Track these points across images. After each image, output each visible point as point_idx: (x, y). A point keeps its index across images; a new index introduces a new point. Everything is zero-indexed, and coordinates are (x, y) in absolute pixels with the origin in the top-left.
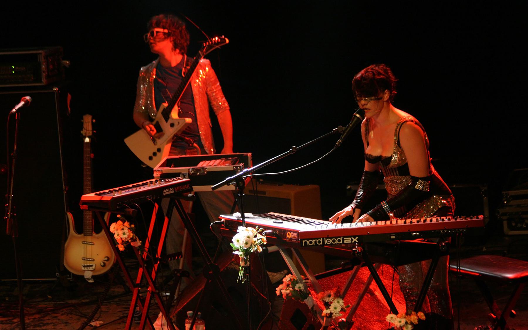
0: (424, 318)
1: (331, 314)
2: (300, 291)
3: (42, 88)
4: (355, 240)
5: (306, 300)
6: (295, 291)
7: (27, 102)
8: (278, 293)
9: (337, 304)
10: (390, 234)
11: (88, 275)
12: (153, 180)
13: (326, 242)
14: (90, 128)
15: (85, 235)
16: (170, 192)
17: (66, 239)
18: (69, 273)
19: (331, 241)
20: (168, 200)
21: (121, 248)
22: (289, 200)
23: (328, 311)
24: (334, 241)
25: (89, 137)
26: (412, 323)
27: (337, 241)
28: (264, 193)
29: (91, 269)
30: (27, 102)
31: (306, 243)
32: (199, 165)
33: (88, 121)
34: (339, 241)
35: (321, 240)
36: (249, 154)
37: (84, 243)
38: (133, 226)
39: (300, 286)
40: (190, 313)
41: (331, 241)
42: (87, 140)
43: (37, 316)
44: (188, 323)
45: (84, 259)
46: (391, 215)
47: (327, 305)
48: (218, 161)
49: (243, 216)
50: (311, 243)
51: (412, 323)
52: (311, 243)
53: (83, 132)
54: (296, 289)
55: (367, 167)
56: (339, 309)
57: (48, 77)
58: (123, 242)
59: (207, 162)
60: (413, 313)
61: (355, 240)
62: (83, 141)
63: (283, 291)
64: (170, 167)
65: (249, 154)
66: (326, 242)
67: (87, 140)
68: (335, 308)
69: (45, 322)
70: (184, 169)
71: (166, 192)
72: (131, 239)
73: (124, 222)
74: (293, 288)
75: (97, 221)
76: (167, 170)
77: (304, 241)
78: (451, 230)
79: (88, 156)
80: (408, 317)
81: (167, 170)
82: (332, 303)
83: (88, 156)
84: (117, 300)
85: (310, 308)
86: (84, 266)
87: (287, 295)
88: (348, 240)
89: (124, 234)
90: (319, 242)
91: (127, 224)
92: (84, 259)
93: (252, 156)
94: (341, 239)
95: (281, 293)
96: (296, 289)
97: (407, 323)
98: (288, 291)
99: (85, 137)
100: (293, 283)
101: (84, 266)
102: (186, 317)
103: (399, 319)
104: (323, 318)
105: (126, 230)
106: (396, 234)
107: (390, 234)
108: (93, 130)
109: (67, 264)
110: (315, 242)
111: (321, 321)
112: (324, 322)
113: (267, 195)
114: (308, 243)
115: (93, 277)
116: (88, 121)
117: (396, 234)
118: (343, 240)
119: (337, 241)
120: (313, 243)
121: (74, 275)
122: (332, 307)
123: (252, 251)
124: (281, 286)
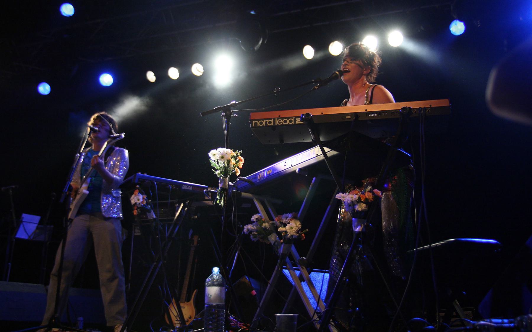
7: (143, 173)
19: (282, 121)
20: (43, 324)
23: (284, 229)
24: (285, 122)
30: (143, 173)
34: (291, 121)
35: (272, 121)
41: (282, 121)
46: (309, 52)
50: (261, 123)
55: (135, 212)
66: (277, 122)
77: (254, 122)
90: (270, 123)
94: (293, 120)
110: (266, 122)
114: (258, 123)
120: (264, 123)
122: (288, 227)
123: (52, 226)
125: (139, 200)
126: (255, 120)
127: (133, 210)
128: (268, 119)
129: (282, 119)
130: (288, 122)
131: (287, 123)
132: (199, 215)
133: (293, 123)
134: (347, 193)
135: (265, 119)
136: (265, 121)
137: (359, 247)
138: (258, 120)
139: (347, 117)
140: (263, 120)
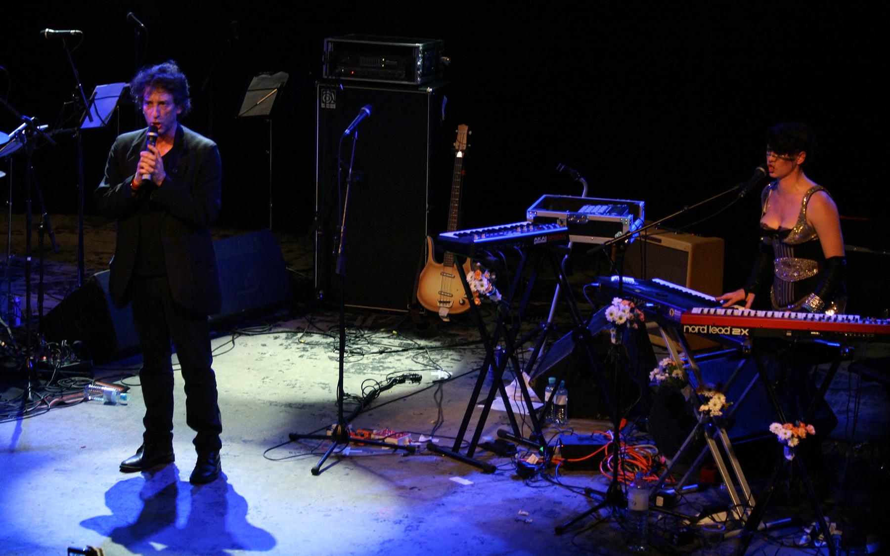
0: (814, 432)
1: (709, 411)
2: (678, 378)
3: (416, 87)
4: (745, 332)
5: (682, 391)
6: (671, 377)
8: (651, 377)
9: (717, 401)
10: (786, 330)
11: (444, 312)
12: (525, 223)
13: (711, 330)
14: (465, 141)
15: (445, 266)
16: (542, 241)
17: (423, 266)
18: (423, 308)
21: (477, 302)
22: (687, 253)
24: (720, 331)
25: (462, 151)
26: (798, 437)
27: (723, 331)
28: (660, 241)
29: (448, 306)
31: (687, 329)
32: (581, 211)
33: (463, 132)
34: (726, 331)
36: (642, 204)
37: (442, 274)
38: (494, 277)
39: (678, 373)
40: (551, 380)
41: (717, 330)
42: (460, 155)
43: (379, 356)
44: (549, 391)
45: (440, 293)
47: (706, 400)
48: (605, 207)
49: (621, 279)
50: (693, 329)
51: (798, 437)
52: (693, 329)
53: (456, 145)
54: (674, 375)
56: (719, 407)
57: (422, 75)
58: (481, 296)
59: (591, 207)
60: (802, 424)
61: (745, 332)
62: (455, 155)
63: (658, 377)
64: (547, 210)
65: (642, 204)
66: (711, 330)
67: (460, 155)
68: (715, 405)
69: (385, 365)
70: (563, 215)
71: (537, 241)
72: (490, 292)
73: (483, 272)
74: (670, 374)
75: (459, 255)
76: (542, 213)
78: (857, 334)
79: (458, 172)
80: (795, 429)
81: (542, 213)
82: (711, 398)
83: (458, 172)
84: (473, 346)
85: (687, 399)
86: (440, 302)
87: (662, 381)
88: (736, 332)
89: (482, 286)
90: (703, 330)
91: (487, 274)
92: (440, 293)
93: (645, 206)
95: (655, 378)
96: (674, 375)
97: (793, 436)
98: (663, 378)
99: (458, 151)
100: (670, 368)
101: (440, 302)
102: (547, 384)
103: (784, 431)
104: (700, 413)
105: (485, 282)
106: (793, 331)
107: (786, 330)
108: (467, 144)
109: (420, 294)
111: (698, 417)
112: (700, 418)
113: (662, 244)
114: (690, 329)
115: (449, 315)
116: (463, 132)
117: (793, 331)
118: (731, 331)
119: (723, 331)
120: (696, 330)
121: (427, 311)
122: (711, 403)
124: (656, 370)
125: (621, 318)
129: (717, 327)
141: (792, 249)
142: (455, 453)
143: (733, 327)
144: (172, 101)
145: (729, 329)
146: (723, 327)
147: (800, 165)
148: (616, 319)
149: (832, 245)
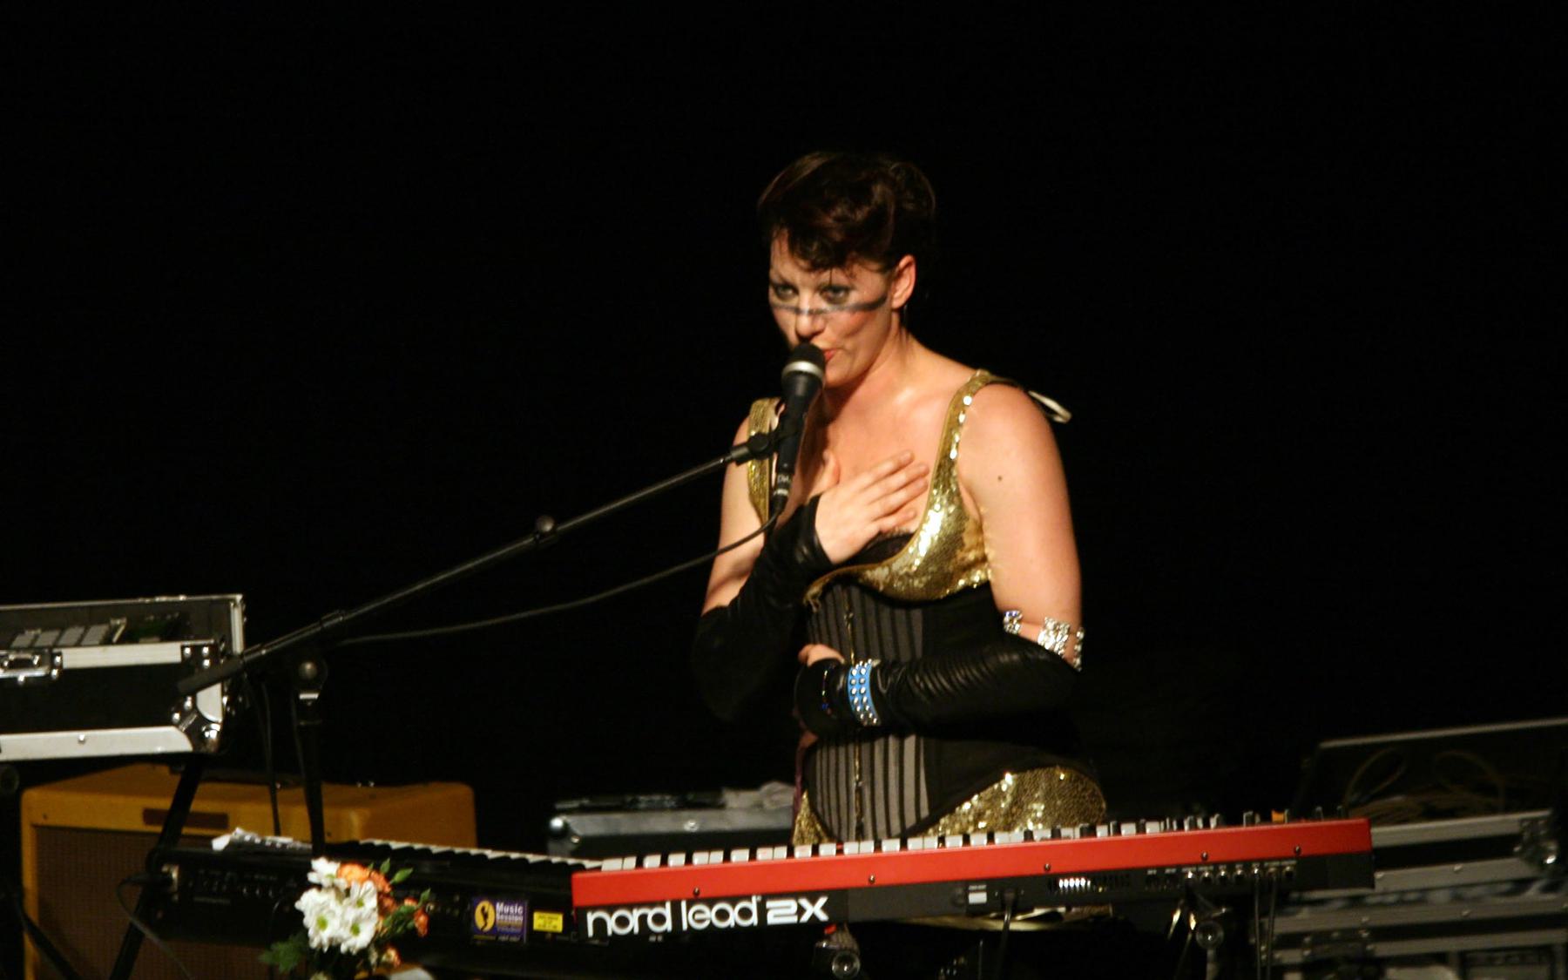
10: (967, 884)
13: (688, 919)
24: (723, 915)
31: (600, 923)
34: (745, 913)
41: (709, 915)
50: (622, 922)
52: (622, 922)
61: (816, 910)
66: (688, 919)
77: (591, 918)
88: (782, 912)
90: (659, 919)
107: (967, 884)
110: (643, 919)
114: (611, 926)
117: (992, 884)
125: (355, 930)
126: (594, 908)
127: (400, 954)
128: (651, 905)
129: (710, 903)
130: (734, 918)
131: (730, 922)
132: (165, 869)
133: (754, 920)
134: (343, 948)
135: (640, 905)
136: (637, 913)
137: (169, 873)
138: (610, 909)
139: (1150, 872)
140: (630, 907)
141: (917, 614)
142: (1030, 844)
143: (767, 896)
144: (203, 750)
145: (667, 911)
146: (733, 901)
147: (900, 310)
148: (345, 933)
149: (1042, 604)
